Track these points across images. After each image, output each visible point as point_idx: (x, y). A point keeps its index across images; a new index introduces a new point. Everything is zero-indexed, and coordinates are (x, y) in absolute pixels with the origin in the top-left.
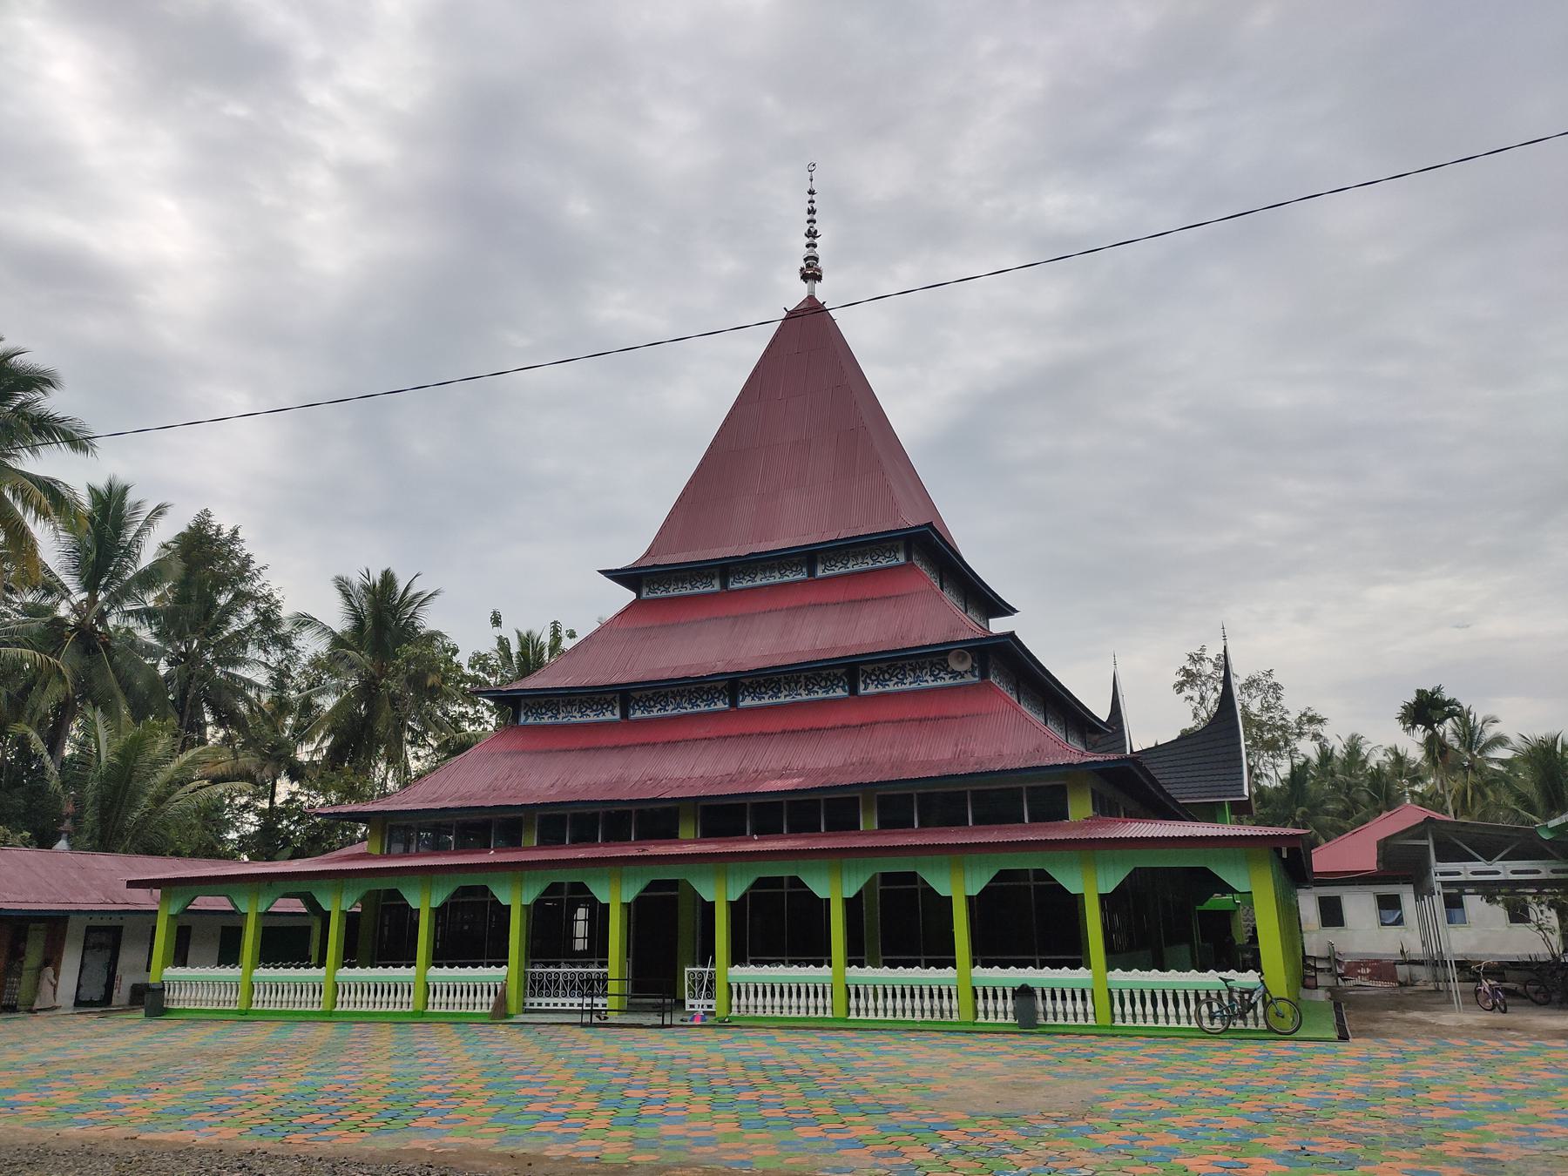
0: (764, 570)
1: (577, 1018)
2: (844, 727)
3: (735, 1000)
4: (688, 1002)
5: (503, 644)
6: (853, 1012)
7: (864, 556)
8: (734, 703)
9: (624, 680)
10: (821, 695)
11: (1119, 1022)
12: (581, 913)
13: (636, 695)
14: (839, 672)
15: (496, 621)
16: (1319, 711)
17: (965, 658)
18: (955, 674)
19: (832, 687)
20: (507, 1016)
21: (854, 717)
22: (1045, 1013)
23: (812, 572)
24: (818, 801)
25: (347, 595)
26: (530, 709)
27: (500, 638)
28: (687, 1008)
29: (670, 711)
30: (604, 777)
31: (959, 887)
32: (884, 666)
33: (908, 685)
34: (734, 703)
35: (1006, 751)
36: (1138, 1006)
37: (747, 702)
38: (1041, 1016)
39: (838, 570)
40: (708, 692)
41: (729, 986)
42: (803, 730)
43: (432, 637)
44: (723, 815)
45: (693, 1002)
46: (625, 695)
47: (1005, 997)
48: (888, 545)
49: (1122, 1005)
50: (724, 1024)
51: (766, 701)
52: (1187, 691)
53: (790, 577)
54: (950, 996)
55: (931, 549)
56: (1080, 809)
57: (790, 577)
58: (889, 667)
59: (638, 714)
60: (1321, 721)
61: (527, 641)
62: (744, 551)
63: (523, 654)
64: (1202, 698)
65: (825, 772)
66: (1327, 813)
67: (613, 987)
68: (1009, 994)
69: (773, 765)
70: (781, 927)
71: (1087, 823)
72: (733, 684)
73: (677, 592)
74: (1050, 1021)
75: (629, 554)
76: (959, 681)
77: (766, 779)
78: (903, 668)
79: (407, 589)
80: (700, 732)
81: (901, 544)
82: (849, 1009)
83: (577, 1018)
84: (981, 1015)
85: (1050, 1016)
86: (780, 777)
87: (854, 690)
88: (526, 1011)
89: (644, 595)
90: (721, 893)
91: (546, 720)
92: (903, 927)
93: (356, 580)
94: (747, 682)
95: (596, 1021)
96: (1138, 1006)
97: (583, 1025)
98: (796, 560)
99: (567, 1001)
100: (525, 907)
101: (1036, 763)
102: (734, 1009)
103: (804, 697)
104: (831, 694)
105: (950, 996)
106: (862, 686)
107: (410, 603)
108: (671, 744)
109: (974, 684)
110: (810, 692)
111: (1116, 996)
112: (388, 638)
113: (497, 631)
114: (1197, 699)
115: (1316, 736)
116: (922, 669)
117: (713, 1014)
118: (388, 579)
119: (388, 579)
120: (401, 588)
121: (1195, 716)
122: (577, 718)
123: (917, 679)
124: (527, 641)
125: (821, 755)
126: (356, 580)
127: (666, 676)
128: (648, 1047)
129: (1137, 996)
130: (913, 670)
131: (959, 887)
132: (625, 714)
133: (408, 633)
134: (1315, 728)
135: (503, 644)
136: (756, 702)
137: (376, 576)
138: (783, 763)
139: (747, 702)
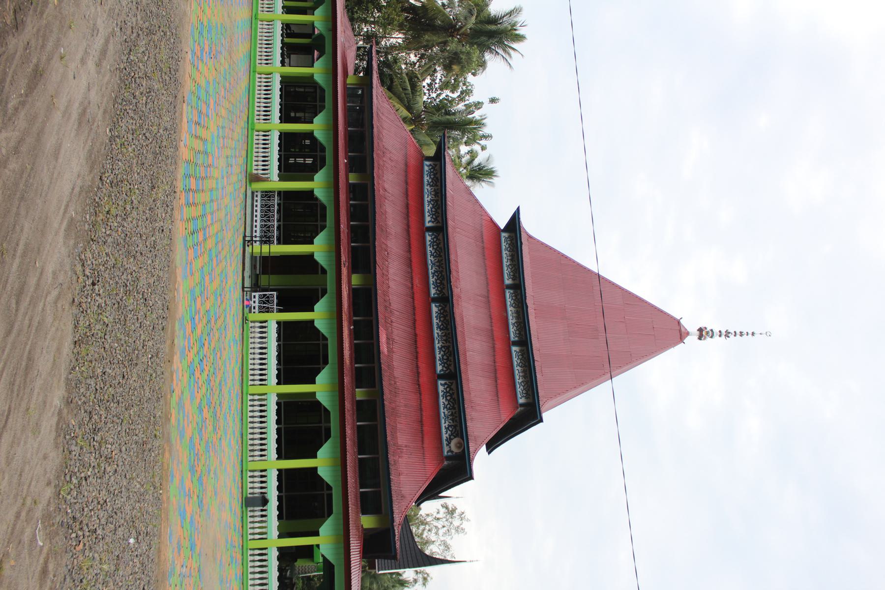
0: (517, 312)
1: (248, 233)
2: (418, 373)
3: (257, 397)
4: (257, 294)
5: (478, 105)
6: (251, 397)
7: (524, 377)
8: (434, 300)
9: (450, 229)
10: (438, 356)
11: (250, 397)
12: (309, 161)
13: (440, 237)
14: (452, 368)
15: (493, 101)
16: (430, 583)
17: (459, 448)
18: (449, 441)
19: (443, 363)
20: (247, 506)
21: (424, 380)
22: (253, 511)
23: (515, 343)
24: (373, 363)
25: (510, 13)
26: (433, 167)
27: (482, 103)
28: (253, 294)
29: (430, 259)
30: (390, 223)
31: (322, 463)
32: (455, 396)
33: (443, 411)
34: (434, 300)
35: (402, 478)
36: (259, 564)
37: (434, 309)
38: (252, 509)
39: (516, 360)
40: (441, 283)
41: (265, 322)
42: (416, 348)
43: (483, 65)
44: (365, 302)
45: (257, 297)
46: (441, 229)
47: (262, 488)
48: (530, 392)
49: (259, 528)
50: (245, 320)
51: (435, 321)
52: (443, 510)
53: (512, 330)
54: (261, 456)
55: (526, 417)
56: (368, 522)
57: (512, 330)
58: (454, 399)
59: (428, 238)
60: (424, 584)
61: (479, 123)
62: (529, 301)
63: (470, 122)
64: (438, 519)
65: (391, 367)
66: (371, 584)
67: (266, 248)
68: (263, 490)
69: (395, 332)
70: (299, 354)
71: (359, 526)
72: (446, 300)
73: (504, 256)
74: (250, 514)
75: (528, 224)
76: (445, 443)
77: (387, 330)
78: (454, 408)
79: (514, 49)
80: (417, 281)
81: (530, 401)
82: (253, 395)
83: (248, 233)
84: (251, 474)
85: (252, 514)
86: (388, 339)
87: (441, 377)
88: (253, 193)
89: (503, 234)
90: (319, 315)
91: (426, 178)
92: (300, 428)
93: (520, 19)
94: (447, 309)
95: (247, 242)
96: (259, 564)
97: (245, 236)
98: (523, 333)
99: (258, 229)
100: (312, 76)
101: (394, 498)
102: (253, 324)
103: (437, 345)
104: (438, 363)
105: (261, 456)
106: (443, 382)
107: (504, 50)
108: (409, 263)
109: (442, 452)
110: (440, 349)
111: (264, 552)
112: (483, 38)
113: (486, 101)
114: (438, 516)
115: (415, 581)
116: (453, 420)
117: (250, 312)
118: (519, 38)
119: (519, 38)
120: (514, 45)
121: (428, 515)
122: (427, 198)
123: (446, 417)
124: (479, 123)
125: (402, 332)
126: (520, 19)
127: (452, 257)
128: (231, 275)
129: (264, 563)
130: (452, 414)
131: (322, 463)
132: (429, 229)
133: (484, 47)
134: (420, 581)
135: (478, 105)
136: (434, 315)
137: (521, 31)
138: (397, 338)
139: (434, 309)
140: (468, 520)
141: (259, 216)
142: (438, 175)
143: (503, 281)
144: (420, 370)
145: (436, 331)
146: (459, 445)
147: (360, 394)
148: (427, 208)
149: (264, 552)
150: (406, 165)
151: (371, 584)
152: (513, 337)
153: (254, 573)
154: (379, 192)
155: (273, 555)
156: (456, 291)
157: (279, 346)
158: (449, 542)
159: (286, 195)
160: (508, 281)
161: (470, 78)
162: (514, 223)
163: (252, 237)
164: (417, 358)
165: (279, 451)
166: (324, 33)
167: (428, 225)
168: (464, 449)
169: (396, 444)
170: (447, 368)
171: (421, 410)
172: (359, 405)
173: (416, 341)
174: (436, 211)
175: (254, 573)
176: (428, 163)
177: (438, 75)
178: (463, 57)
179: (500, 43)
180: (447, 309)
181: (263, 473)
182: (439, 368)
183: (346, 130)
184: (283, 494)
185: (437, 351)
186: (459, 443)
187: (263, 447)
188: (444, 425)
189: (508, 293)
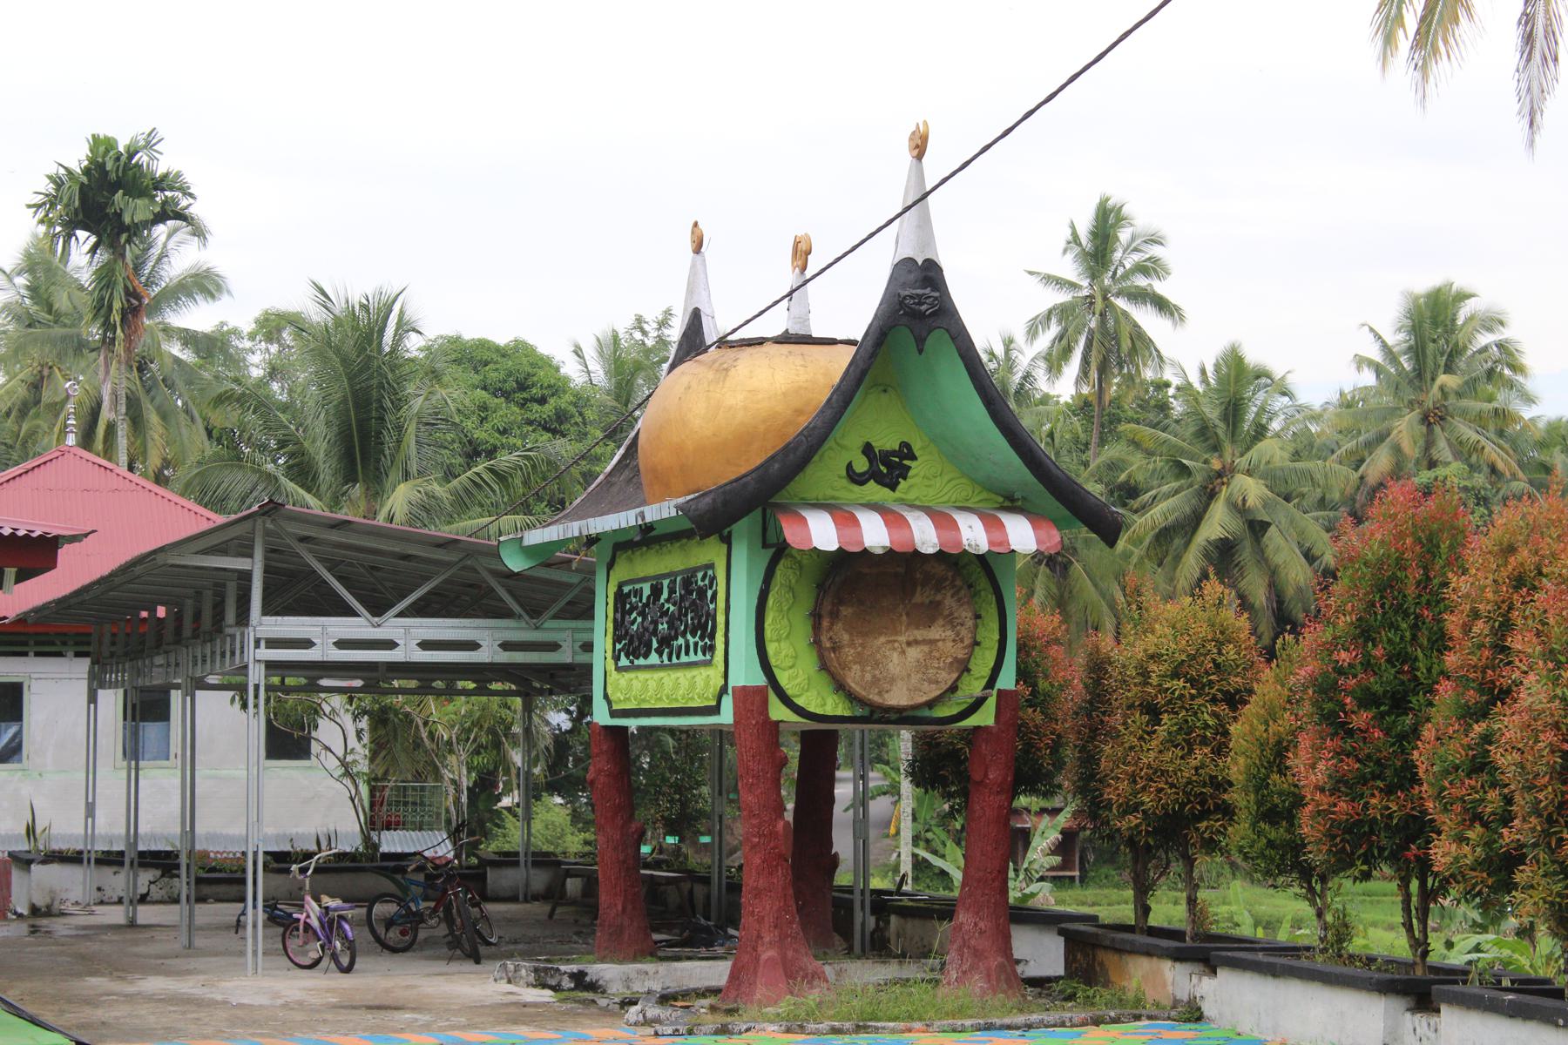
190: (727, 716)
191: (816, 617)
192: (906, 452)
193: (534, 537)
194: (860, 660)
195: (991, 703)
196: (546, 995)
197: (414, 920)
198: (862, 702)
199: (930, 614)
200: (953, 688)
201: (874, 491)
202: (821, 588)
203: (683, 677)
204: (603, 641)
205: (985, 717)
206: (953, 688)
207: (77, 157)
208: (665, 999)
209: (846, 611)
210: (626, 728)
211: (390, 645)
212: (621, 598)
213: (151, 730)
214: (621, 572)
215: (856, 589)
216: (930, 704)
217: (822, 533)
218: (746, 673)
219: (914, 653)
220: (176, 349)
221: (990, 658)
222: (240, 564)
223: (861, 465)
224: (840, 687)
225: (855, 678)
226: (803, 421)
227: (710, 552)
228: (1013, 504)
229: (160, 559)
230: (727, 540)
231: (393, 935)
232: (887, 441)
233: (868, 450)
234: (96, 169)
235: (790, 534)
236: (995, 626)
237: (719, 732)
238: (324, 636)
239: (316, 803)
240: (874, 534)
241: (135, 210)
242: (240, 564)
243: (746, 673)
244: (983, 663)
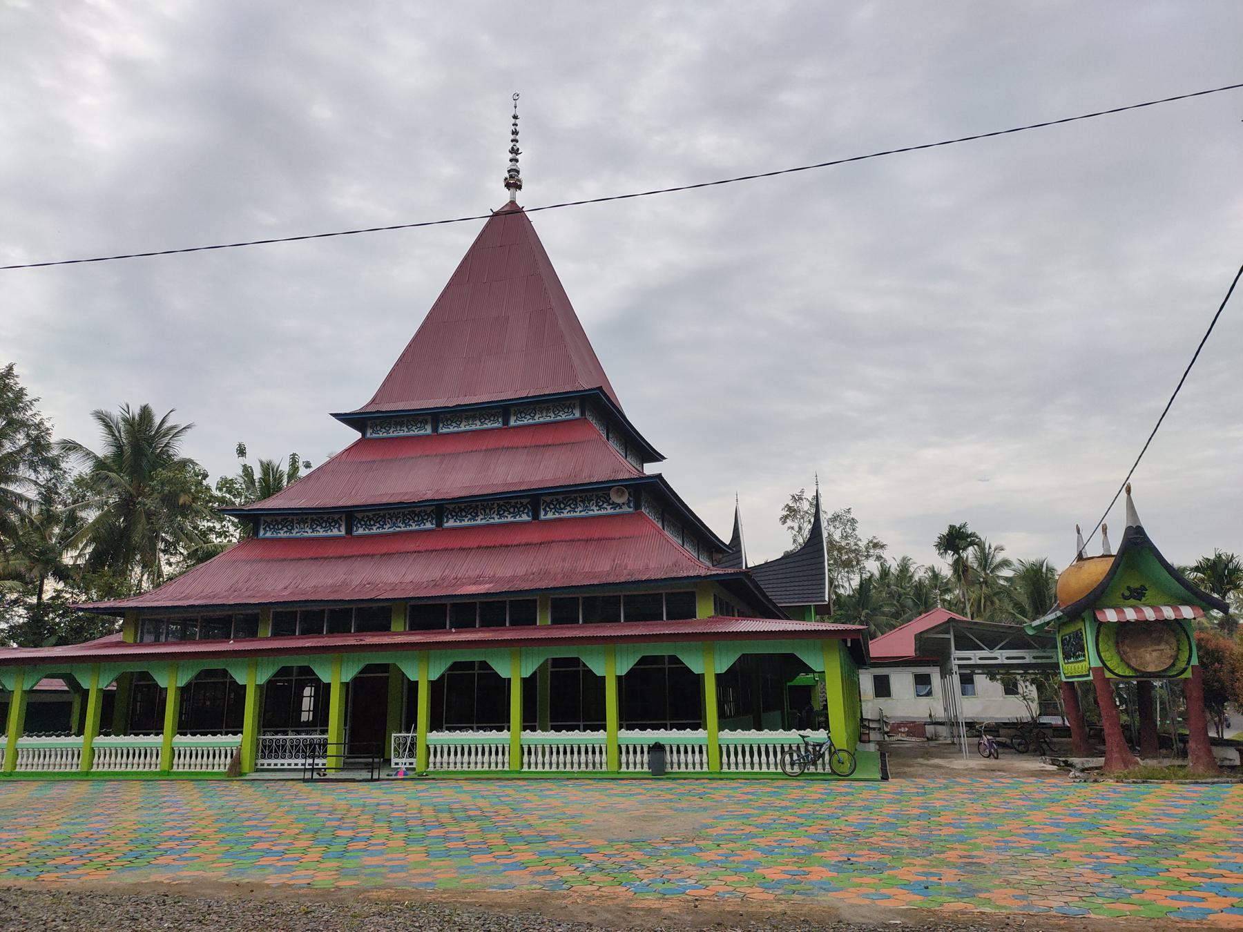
0: (467, 419)
1: (301, 775)
4: (394, 761)
5: (247, 471)
7: (548, 410)
10: (510, 519)
13: (360, 516)
14: (525, 501)
15: (241, 452)
16: (881, 539)
19: (519, 513)
20: (241, 774)
23: (506, 422)
26: (268, 525)
27: (245, 466)
29: (387, 529)
31: (610, 669)
32: (560, 498)
36: (740, 757)
37: (451, 523)
40: (418, 515)
41: (428, 747)
43: (184, 463)
45: (397, 760)
46: (350, 515)
50: (422, 777)
51: (466, 523)
52: (789, 523)
53: (488, 425)
54: (601, 752)
55: (600, 407)
56: (705, 610)
57: (488, 425)
59: (361, 531)
60: (883, 547)
63: (265, 479)
64: (800, 528)
66: (883, 614)
67: (332, 750)
68: (646, 750)
69: (470, 573)
70: (471, 700)
71: (710, 621)
72: (439, 509)
74: (675, 769)
75: (357, 401)
76: (618, 510)
77: (463, 584)
78: (575, 499)
80: (411, 546)
81: (577, 402)
82: (522, 764)
83: (301, 775)
85: (675, 766)
87: (536, 516)
88: (257, 771)
89: (368, 435)
91: (282, 534)
92: (566, 699)
95: (316, 777)
96: (740, 757)
97: (305, 780)
99: (293, 761)
100: (259, 687)
101: (673, 575)
102: (431, 765)
104: (518, 519)
105: (601, 752)
106: (542, 513)
111: (724, 750)
113: (242, 461)
114: (796, 528)
115: (879, 558)
117: (414, 769)
118: (146, 413)
119: (146, 413)
121: (795, 541)
123: (586, 508)
124: (267, 468)
126: (116, 413)
127: (384, 501)
128: (361, 797)
129: (763, 749)
130: (583, 501)
131: (610, 669)
133: (164, 460)
134: (878, 551)
135: (247, 471)
136: (458, 524)
137: (136, 410)
138: (477, 572)
139: (451, 523)
140: (802, 492)
141: (276, 761)
142: (279, 519)
143: (428, 436)
144: (524, 542)
145: (479, 521)
146: (620, 493)
147: (544, 618)
148: (321, 533)
149: (724, 750)
150: (261, 560)
151: (883, 614)
152: (498, 425)
153: (752, 764)
154: (286, 596)
155: (727, 735)
156: (429, 496)
157: (449, 729)
158: (830, 516)
159: (267, 722)
160: (428, 430)
161: (212, 482)
162: (350, 419)
163: (305, 770)
164: (507, 546)
165: (695, 727)
166: (115, 674)
167: (343, 533)
168: (625, 486)
169: (608, 574)
170: (525, 507)
171: (572, 541)
172: (556, 621)
173: (487, 547)
174: (326, 522)
175: (752, 764)
176: (262, 533)
177: (204, 525)
178: (167, 488)
179: (151, 441)
180: (451, 507)
181: (624, 749)
182: (525, 518)
183: (198, 643)
184: (581, 724)
185: (503, 520)
186: (618, 491)
187: (590, 750)
188: (596, 512)
189: (443, 430)
190: (1091, 678)
191: (1117, 644)
192: (1143, 588)
193: (1036, 623)
194: (1135, 657)
195: (1190, 669)
196: (1055, 767)
197: (1027, 745)
198: (1135, 670)
199: (1159, 641)
200: (1173, 665)
201: (1132, 601)
202: (1117, 634)
203: (1079, 665)
204: (1061, 656)
205: (1188, 674)
206: (1173, 665)
207: (945, 531)
208: (1083, 770)
209: (1127, 641)
210: (21, 645)
211: (996, 658)
212: (1062, 641)
213: (969, 686)
214: (1062, 633)
215: (1125, 633)
216: (1165, 671)
217: (1111, 616)
218: (1095, 663)
219: (1154, 654)
220: (1002, 582)
221: (1187, 654)
222: (947, 636)
223: (1127, 593)
224: (1129, 666)
225: (1133, 663)
226: (1101, 578)
227: (1080, 625)
228: (1186, 602)
229: (926, 636)
230: (1084, 620)
231: (1021, 748)
232: (1135, 585)
233: (1128, 588)
234: (950, 534)
235: (1100, 617)
236: (1186, 643)
237: (1091, 682)
238: (975, 657)
239: (1019, 707)
240: (1130, 615)
241: (962, 544)
242: (947, 636)
243: (1095, 663)
244: (1184, 656)
